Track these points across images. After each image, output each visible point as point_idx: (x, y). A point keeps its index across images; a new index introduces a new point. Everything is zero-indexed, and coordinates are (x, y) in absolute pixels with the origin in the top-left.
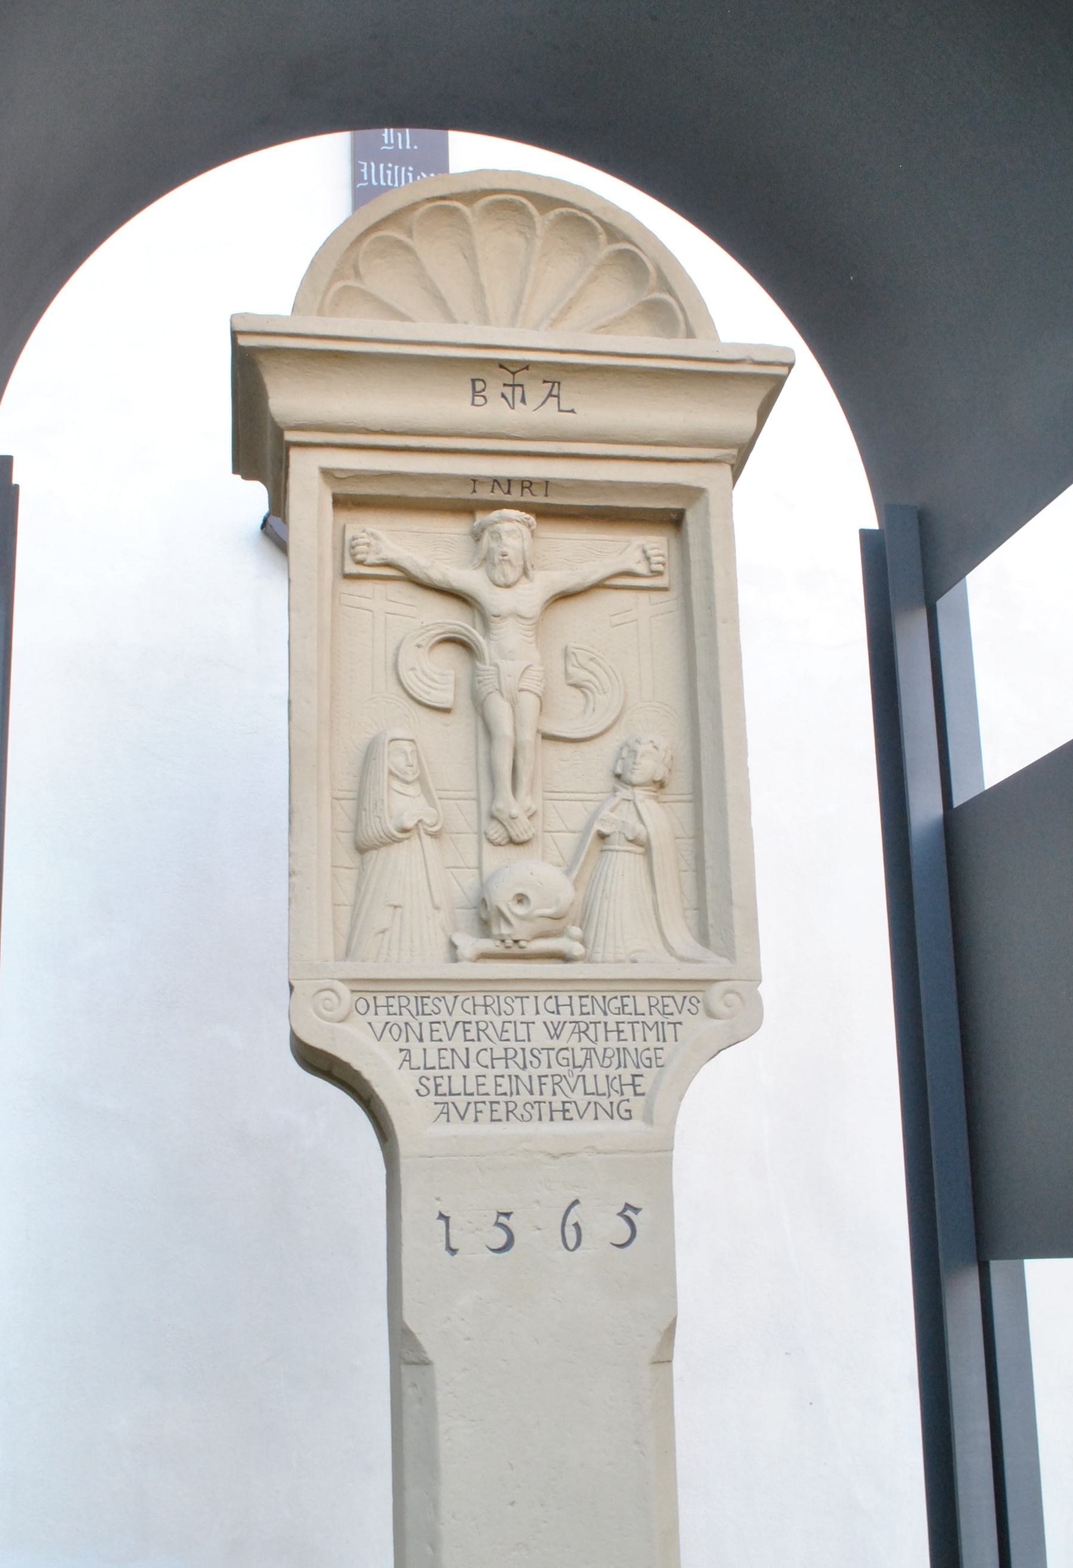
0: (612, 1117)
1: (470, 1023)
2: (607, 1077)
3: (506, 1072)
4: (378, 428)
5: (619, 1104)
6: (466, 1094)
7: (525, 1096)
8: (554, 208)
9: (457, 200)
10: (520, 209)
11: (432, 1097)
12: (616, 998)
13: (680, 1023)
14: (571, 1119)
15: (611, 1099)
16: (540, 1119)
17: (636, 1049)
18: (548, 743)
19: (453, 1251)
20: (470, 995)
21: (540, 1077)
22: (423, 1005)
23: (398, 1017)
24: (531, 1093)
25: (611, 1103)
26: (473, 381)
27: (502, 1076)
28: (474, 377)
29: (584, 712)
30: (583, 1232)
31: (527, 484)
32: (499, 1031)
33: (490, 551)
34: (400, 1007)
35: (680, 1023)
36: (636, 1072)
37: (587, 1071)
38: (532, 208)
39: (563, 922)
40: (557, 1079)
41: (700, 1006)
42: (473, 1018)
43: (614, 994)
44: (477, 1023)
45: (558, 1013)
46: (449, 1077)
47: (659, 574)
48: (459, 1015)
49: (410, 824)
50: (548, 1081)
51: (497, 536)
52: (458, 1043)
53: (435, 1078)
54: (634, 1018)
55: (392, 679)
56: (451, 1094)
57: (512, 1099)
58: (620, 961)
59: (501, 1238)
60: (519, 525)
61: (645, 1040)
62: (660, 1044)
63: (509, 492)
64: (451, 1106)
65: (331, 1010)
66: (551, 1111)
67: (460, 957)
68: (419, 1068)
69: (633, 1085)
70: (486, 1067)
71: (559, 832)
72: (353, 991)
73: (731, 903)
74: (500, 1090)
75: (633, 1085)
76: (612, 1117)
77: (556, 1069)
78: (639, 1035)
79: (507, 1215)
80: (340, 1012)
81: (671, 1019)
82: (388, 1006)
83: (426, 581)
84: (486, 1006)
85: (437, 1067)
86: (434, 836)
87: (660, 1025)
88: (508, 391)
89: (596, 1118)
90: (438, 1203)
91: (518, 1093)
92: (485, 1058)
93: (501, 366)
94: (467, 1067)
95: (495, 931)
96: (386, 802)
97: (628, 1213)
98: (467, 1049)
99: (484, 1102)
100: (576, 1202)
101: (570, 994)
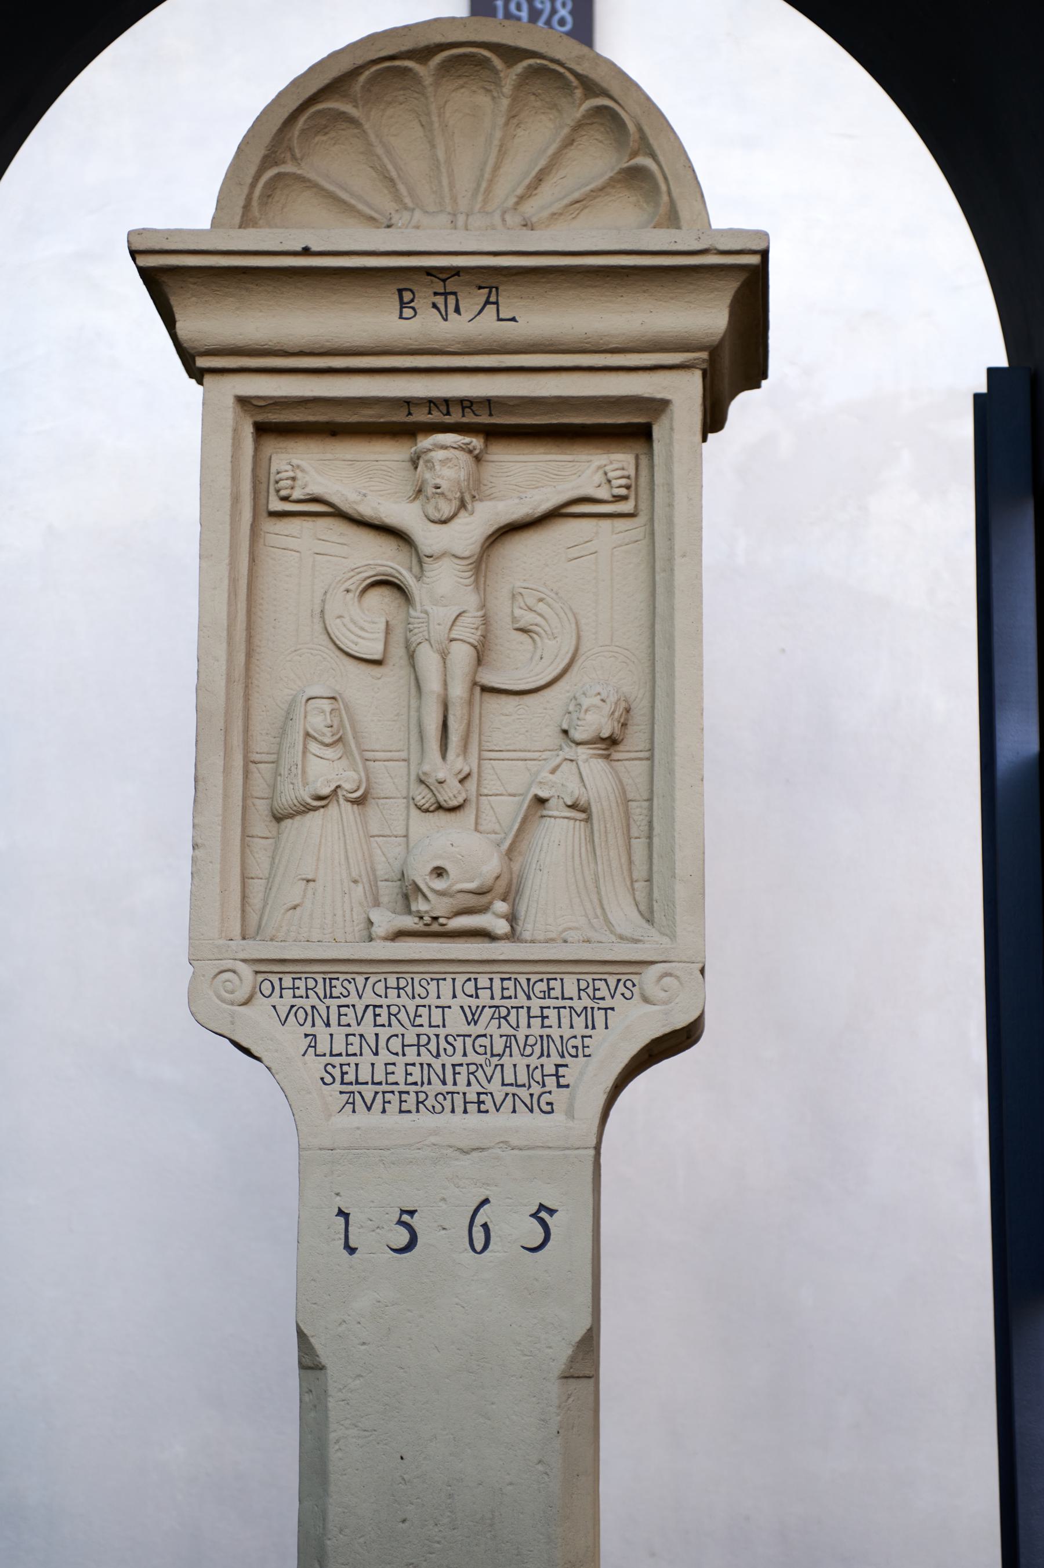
0: (531, 1111)
1: (381, 1006)
2: (528, 1066)
3: (418, 1060)
4: (297, 350)
5: (540, 1096)
6: (373, 1083)
7: (437, 1086)
8: (521, 60)
9: (409, 58)
10: (483, 63)
11: (337, 1086)
12: (542, 980)
13: (612, 1009)
14: (487, 1112)
15: (531, 1091)
16: (453, 1111)
17: (561, 1037)
18: (487, 696)
19: (352, 1250)
20: (382, 977)
21: (454, 1066)
22: (331, 987)
23: (304, 1000)
24: (444, 1083)
25: (531, 1095)
26: (400, 291)
27: (414, 1065)
28: (401, 287)
29: (532, 659)
30: (492, 1234)
31: (466, 404)
32: (412, 1016)
33: (424, 482)
34: (307, 989)
35: (612, 1009)
36: (560, 1061)
37: (506, 1060)
38: (497, 62)
39: (489, 897)
40: (473, 1068)
41: (635, 990)
42: (384, 1002)
43: (540, 977)
44: (389, 1007)
45: (477, 997)
46: (357, 1065)
47: (625, 498)
48: (369, 998)
49: (325, 791)
50: (463, 1070)
51: (430, 465)
52: (367, 1028)
53: (341, 1065)
54: (560, 1003)
55: (318, 627)
56: (357, 1083)
57: (423, 1089)
58: (553, 940)
59: (402, 1237)
60: (457, 453)
61: (572, 1027)
62: (589, 1032)
63: (448, 413)
64: (357, 1095)
65: (232, 992)
66: (465, 1103)
67: (374, 936)
68: (324, 1055)
69: (557, 1076)
70: (397, 1054)
71: (497, 795)
72: (257, 972)
73: (674, 876)
74: (410, 1079)
75: (557, 1076)
76: (531, 1111)
77: (472, 1057)
78: (565, 1021)
79: (411, 1213)
80: (242, 994)
81: (603, 1004)
82: (294, 988)
83: (356, 516)
84: (398, 988)
85: (344, 1054)
86: (359, 802)
87: (589, 1010)
88: (440, 301)
89: (514, 1111)
90: (338, 1198)
91: (429, 1083)
92: (396, 1044)
93: (429, 274)
94: (376, 1054)
95: (414, 908)
96: (300, 766)
97: (542, 1213)
98: (377, 1035)
99: (393, 1092)
100: (486, 1201)
101: (491, 976)
